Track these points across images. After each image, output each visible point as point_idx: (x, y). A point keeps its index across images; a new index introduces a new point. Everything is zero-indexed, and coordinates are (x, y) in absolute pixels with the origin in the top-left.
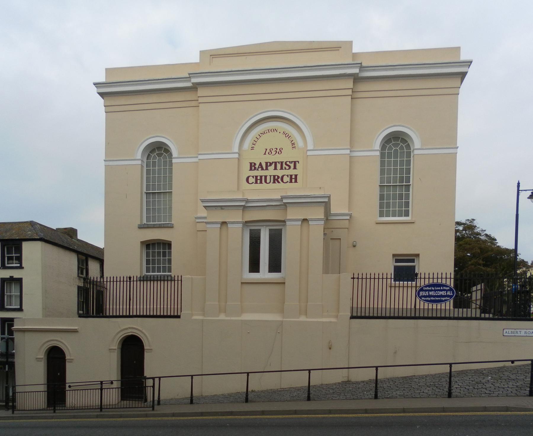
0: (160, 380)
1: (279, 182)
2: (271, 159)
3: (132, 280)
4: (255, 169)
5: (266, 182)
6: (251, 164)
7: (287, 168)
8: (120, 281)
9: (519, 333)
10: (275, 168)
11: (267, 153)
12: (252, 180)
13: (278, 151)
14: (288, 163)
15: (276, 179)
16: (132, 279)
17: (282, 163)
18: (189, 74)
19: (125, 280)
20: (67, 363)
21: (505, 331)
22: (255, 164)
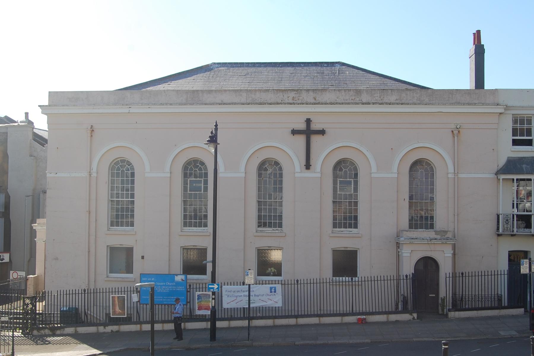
8: (69, 294)
19: (80, 292)
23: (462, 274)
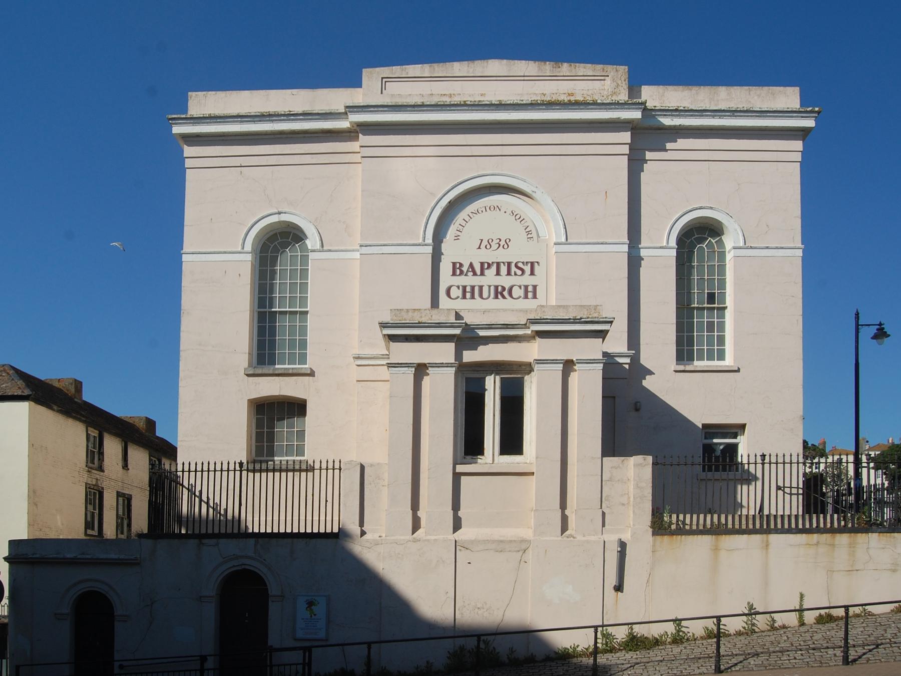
0: (369, 648)
1: (504, 297)
4: (462, 272)
5: (481, 296)
6: (454, 264)
7: (519, 272)
10: (498, 273)
11: (483, 246)
12: (455, 292)
13: (502, 243)
14: (520, 265)
15: (499, 292)
16: (767, 458)
17: (509, 264)
18: (347, 107)
19: (232, 468)
20: (116, 623)
22: (461, 265)
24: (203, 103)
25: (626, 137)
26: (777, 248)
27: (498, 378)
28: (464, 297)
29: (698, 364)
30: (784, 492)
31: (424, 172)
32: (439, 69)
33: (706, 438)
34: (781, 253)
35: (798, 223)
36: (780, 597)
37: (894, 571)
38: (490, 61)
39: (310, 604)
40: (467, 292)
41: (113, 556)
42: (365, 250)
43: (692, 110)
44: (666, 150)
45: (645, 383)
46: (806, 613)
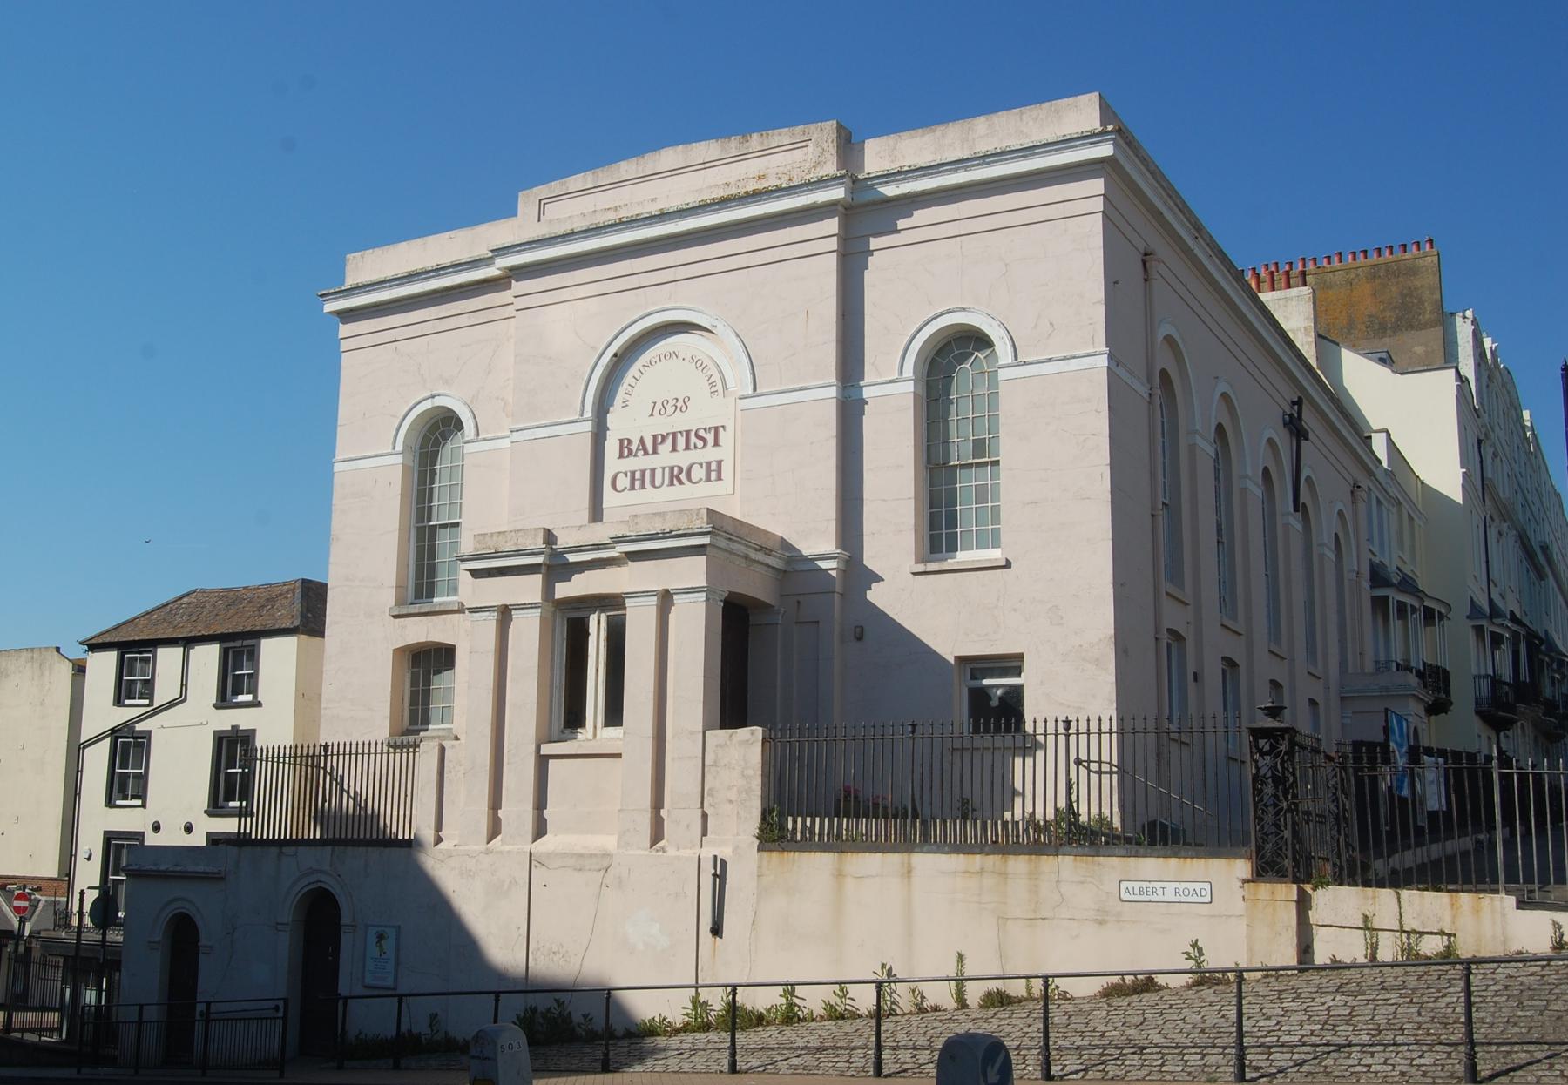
0: (497, 1000)
1: (681, 482)
2: (663, 425)
3: (1073, 730)
6: (621, 441)
7: (700, 444)
9: (1160, 891)
10: (674, 449)
13: (680, 404)
14: (702, 433)
15: (676, 476)
16: (1073, 725)
17: (688, 433)
21: (1124, 885)
22: (630, 442)
23: (1067, 723)
24: (370, 266)
25: (832, 225)
26: (1065, 358)
27: (603, 616)
28: (633, 488)
29: (963, 557)
30: (1089, 771)
31: (576, 322)
32: (604, 175)
33: (973, 677)
34: (1073, 365)
35: (1099, 313)
36: (1161, 954)
37: (1101, 922)
38: (663, 151)
39: (381, 937)
40: (638, 480)
41: (201, 868)
42: (517, 436)
43: (922, 168)
44: (899, 231)
45: (870, 596)
46: (967, 983)
